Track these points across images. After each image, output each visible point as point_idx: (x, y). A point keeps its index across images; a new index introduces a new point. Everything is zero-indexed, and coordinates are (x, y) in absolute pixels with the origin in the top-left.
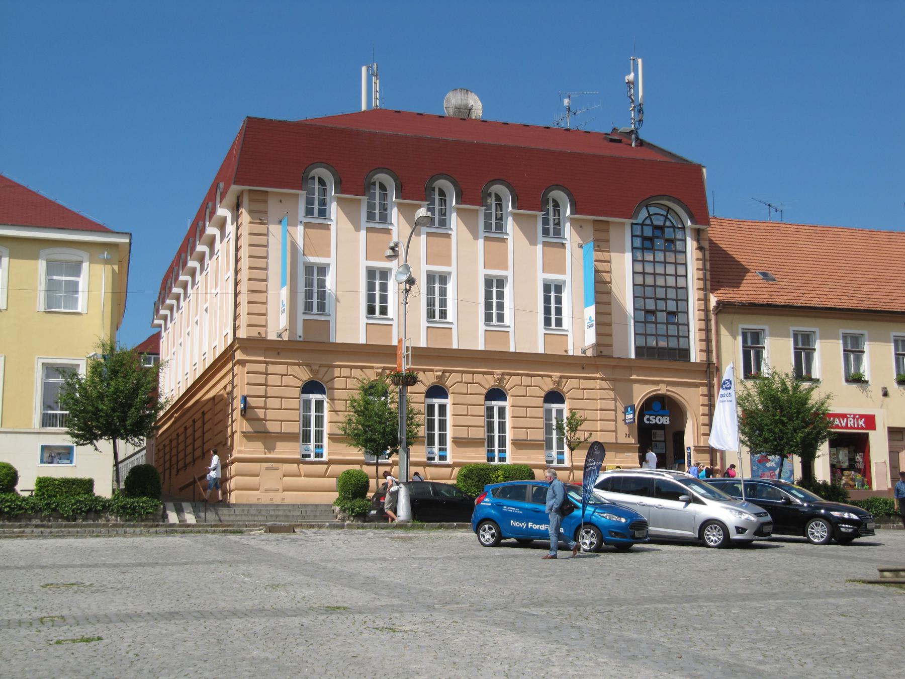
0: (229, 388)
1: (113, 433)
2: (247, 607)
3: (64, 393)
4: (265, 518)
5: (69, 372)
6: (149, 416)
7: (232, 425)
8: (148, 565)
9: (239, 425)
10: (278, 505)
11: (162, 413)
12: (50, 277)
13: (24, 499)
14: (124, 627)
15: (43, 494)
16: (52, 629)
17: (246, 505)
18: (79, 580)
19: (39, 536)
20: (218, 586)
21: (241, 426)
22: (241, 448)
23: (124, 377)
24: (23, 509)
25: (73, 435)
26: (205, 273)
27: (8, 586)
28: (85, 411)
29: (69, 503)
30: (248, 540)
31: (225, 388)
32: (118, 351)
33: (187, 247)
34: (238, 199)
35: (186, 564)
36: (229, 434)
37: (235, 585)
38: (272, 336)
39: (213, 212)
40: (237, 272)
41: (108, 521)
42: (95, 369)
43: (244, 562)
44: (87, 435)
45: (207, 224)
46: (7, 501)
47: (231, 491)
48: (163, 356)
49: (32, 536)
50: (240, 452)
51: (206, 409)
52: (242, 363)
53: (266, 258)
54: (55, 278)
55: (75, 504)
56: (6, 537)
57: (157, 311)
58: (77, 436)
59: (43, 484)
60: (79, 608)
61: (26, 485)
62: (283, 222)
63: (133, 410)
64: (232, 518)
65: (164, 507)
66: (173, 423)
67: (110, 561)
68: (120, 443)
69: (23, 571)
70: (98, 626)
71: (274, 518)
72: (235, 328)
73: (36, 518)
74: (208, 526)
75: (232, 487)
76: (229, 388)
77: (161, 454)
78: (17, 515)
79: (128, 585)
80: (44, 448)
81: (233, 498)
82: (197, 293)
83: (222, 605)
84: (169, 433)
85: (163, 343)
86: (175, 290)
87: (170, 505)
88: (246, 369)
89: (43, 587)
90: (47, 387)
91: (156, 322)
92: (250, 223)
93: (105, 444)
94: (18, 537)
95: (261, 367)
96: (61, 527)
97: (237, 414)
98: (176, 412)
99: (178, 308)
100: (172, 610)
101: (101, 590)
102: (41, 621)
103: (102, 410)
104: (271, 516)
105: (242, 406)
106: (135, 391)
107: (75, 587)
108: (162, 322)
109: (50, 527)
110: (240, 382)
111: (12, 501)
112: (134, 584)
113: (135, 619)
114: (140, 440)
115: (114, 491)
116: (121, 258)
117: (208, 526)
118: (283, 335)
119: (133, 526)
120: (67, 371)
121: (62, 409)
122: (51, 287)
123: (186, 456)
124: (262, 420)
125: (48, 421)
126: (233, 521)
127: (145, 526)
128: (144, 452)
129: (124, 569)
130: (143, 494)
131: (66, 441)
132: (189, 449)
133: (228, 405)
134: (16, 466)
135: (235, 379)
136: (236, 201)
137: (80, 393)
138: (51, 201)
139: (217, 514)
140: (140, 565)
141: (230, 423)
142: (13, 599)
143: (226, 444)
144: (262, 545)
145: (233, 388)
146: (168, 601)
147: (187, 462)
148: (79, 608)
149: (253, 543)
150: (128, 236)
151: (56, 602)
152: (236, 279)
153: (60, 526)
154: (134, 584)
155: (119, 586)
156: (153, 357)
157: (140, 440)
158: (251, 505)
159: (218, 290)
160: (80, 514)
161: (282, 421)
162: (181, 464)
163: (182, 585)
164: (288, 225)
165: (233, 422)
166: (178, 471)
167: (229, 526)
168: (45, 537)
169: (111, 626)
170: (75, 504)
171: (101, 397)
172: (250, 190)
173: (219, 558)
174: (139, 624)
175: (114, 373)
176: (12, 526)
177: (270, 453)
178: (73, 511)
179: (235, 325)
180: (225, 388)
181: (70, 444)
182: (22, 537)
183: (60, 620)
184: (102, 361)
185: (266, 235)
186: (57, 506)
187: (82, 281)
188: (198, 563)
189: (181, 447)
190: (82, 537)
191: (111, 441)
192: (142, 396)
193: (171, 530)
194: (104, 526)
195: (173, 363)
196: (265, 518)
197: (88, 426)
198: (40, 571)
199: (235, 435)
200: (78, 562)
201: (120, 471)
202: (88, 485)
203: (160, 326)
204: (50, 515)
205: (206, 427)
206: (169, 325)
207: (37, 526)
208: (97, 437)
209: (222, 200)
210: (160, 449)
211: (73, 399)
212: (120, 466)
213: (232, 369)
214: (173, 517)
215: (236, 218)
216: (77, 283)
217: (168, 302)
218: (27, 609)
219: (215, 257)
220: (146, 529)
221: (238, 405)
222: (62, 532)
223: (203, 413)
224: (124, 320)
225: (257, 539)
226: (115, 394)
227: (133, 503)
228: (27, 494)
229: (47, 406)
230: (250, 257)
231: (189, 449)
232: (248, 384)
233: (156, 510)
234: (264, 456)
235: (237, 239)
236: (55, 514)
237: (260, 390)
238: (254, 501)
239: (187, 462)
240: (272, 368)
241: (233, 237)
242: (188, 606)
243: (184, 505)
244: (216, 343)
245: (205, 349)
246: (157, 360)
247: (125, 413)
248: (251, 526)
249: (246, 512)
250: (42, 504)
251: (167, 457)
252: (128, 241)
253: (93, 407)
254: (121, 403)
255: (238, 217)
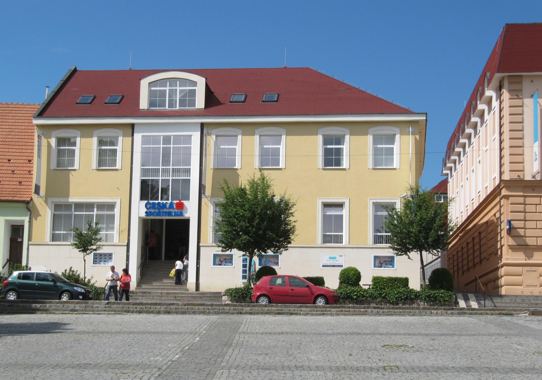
0: (498, 215)
1: (420, 247)
2: (522, 366)
3: (387, 221)
4: (528, 306)
5: (390, 207)
6: (442, 235)
7: (501, 240)
8: (449, 335)
9: (506, 241)
10: (537, 296)
11: (451, 233)
12: (375, 146)
13: (365, 291)
14: (438, 375)
15: (377, 287)
16: (391, 374)
17: (513, 296)
18: (405, 343)
19: (376, 314)
20: (499, 351)
21: (508, 241)
22: (508, 256)
23: (426, 210)
24: (364, 297)
25: (394, 249)
26: (477, 136)
27: (361, 345)
28: (401, 233)
29: (393, 293)
30: (517, 320)
31: (495, 215)
32: (421, 192)
33: (465, 120)
34: (500, 83)
35: (475, 335)
36: (499, 246)
37: (511, 351)
38: (528, 177)
39: (483, 93)
40: (501, 134)
41: (419, 305)
42: (407, 205)
43: (516, 335)
44: (403, 248)
45: (478, 102)
46: (355, 292)
47: (502, 286)
48: (450, 194)
49: (372, 314)
50: (507, 259)
51: (481, 230)
52: (507, 197)
53: (522, 122)
54: (379, 146)
55: (397, 294)
56: (356, 314)
57: (445, 165)
58: (396, 249)
59: (377, 281)
60: (407, 361)
61: (366, 282)
62: (534, 96)
63: (432, 231)
64: (504, 305)
65: (456, 297)
66: (459, 240)
67: (423, 332)
68: (424, 253)
69: (369, 336)
70: (421, 373)
71: (534, 306)
72: (501, 174)
73: (373, 303)
74: (487, 310)
75: (503, 283)
76: (498, 215)
77: (451, 261)
78: (361, 301)
79: (437, 348)
80: (376, 257)
81: (503, 291)
82: (473, 151)
83: (503, 364)
84: (456, 247)
85: (450, 186)
86: (457, 150)
87: (460, 295)
88: (510, 202)
89: (382, 347)
90: (376, 218)
91: (445, 172)
92: (510, 99)
93: (414, 255)
94: (363, 314)
95: (521, 200)
96: (390, 309)
97: (504, 233)
98: (460, 232)
99: (460, 162)
100: (469, 366)
101: (419, 350)
102: (384, 368)
103: (412, 232)
104: (532, 304)
105: (508, 227)
106: (433, 220)
107: (403, 348)
108: (449, 172)
109: (383, 309)
110: (506, 211)
111: (358, 292)
112: (441, 348)
113: (444, 370)
114: (438, 251)
115: (421, 286)
116: (421, 130)
117: (487, 310)
118: (536, 176)
119: (436, 309)
120: (389, 207)
121: (386, 232)
122: (377, 152)
123: (468, 262)
124: (523, 236)
125: (378, 240)
126: (504, 307)
127: (444, 309)
128: (439, 260)
129: (433, 337)
130: (441, 288)
131: (390, 253)
132: (471, 258)
133: (497, 227)
134: (359, 269)
135: (502, 209)
136: (498, 84)
137: (397, 221)
138: (374, 96)
139: (493, 302)
140: (443, 335)
141: (499, 239)
142: (365, 354)
143: (497, 253)
144: (528, 324)
145: (501, 215)
146: (465, 360)
147: (469, 266)
148: (407, 361)
149: (521, 322)
150: (425, 115)
151: (392, 357)
152: (500, 139)
153: (388, 308)
154: (441, 348)
155: (431, 348)
156: (442, 196)
157: (438, 251)
158: (517, 296)
159: (488, 147)
160: (401, 300)
161: (537, 237)
162: (465, 268)
163: (473, 349)
164: (539, 97)
165: (501, 238)
166: (463, 272)
167: (503, 310)
168: (380, 315)
169: (429, 374)
170: (397, 294)
171: (411, 223)
172: (509, 76)
173: (498, 332)
174: (448, 374)
175: (420, 207)
176: (360, 308)
177: (529, 259)
178: (396, 298)
179: (500, 171)
180: (495, 215)
181: (392, 255)
182: (366, 314)
183: (395, 368)
184: (411, 199)
185: (522, 106)
186: (385, 295)
187: (396, 147)
188: (483, 335)
189: (465, 256)
190: (403, 315)
191: (419, 252)
192: (438, 222)
193: (462, 312)
194: (417, 308)
195: (457, 199)
196: (528, 306)
197: (403, 243)
198: (379, 336)
199: (503, 248)
200: (403, 332)
201: (425, 271)
202: (405, 282)
203: (447, 174)
204: (382, 301)
205: (483, 242)
206: (453, 173)
207: (374, 308)
208: (409, 250)
209: (488, 86)
210: (451, 258)
211: (392, 225)
212: (425, 268)
213: (500, 202)
214: (462, 304)
215: (499, 96)
216: (392, 149)
217: (453, 158)
218: (374, 360)
219: (485, 125)
220: (445, 311)
221: (505, 226)
222: (391, 312)
223: (480, 233)
224: (423, 171)
225: (523, 319)
226: (420, 221)
227: (435, 294)
228: (367, 287)
229: (376, 230)
230: (510, 123)
231: (471, 258)
232: (512, 212)
233: (450, 298)
234: (524, 262)
235: (501, 111)
236: (385, 300)
237: (521, 216)
238: (519, 293)
239: (469, 266)
240: (529, 200)
241: (497, 110)
242: (479, 363)
243: (469, 295)
244: (488, 184)
245: (480, 188)
246: (446, 198)
247: (427, 234)
248: (518, 310)
249: (513, 301)
250: (376, 294)
251: (456, 263)
252: (425, 118)
253: (406, 230)
254: (424, 227)
255: (501, 95)
